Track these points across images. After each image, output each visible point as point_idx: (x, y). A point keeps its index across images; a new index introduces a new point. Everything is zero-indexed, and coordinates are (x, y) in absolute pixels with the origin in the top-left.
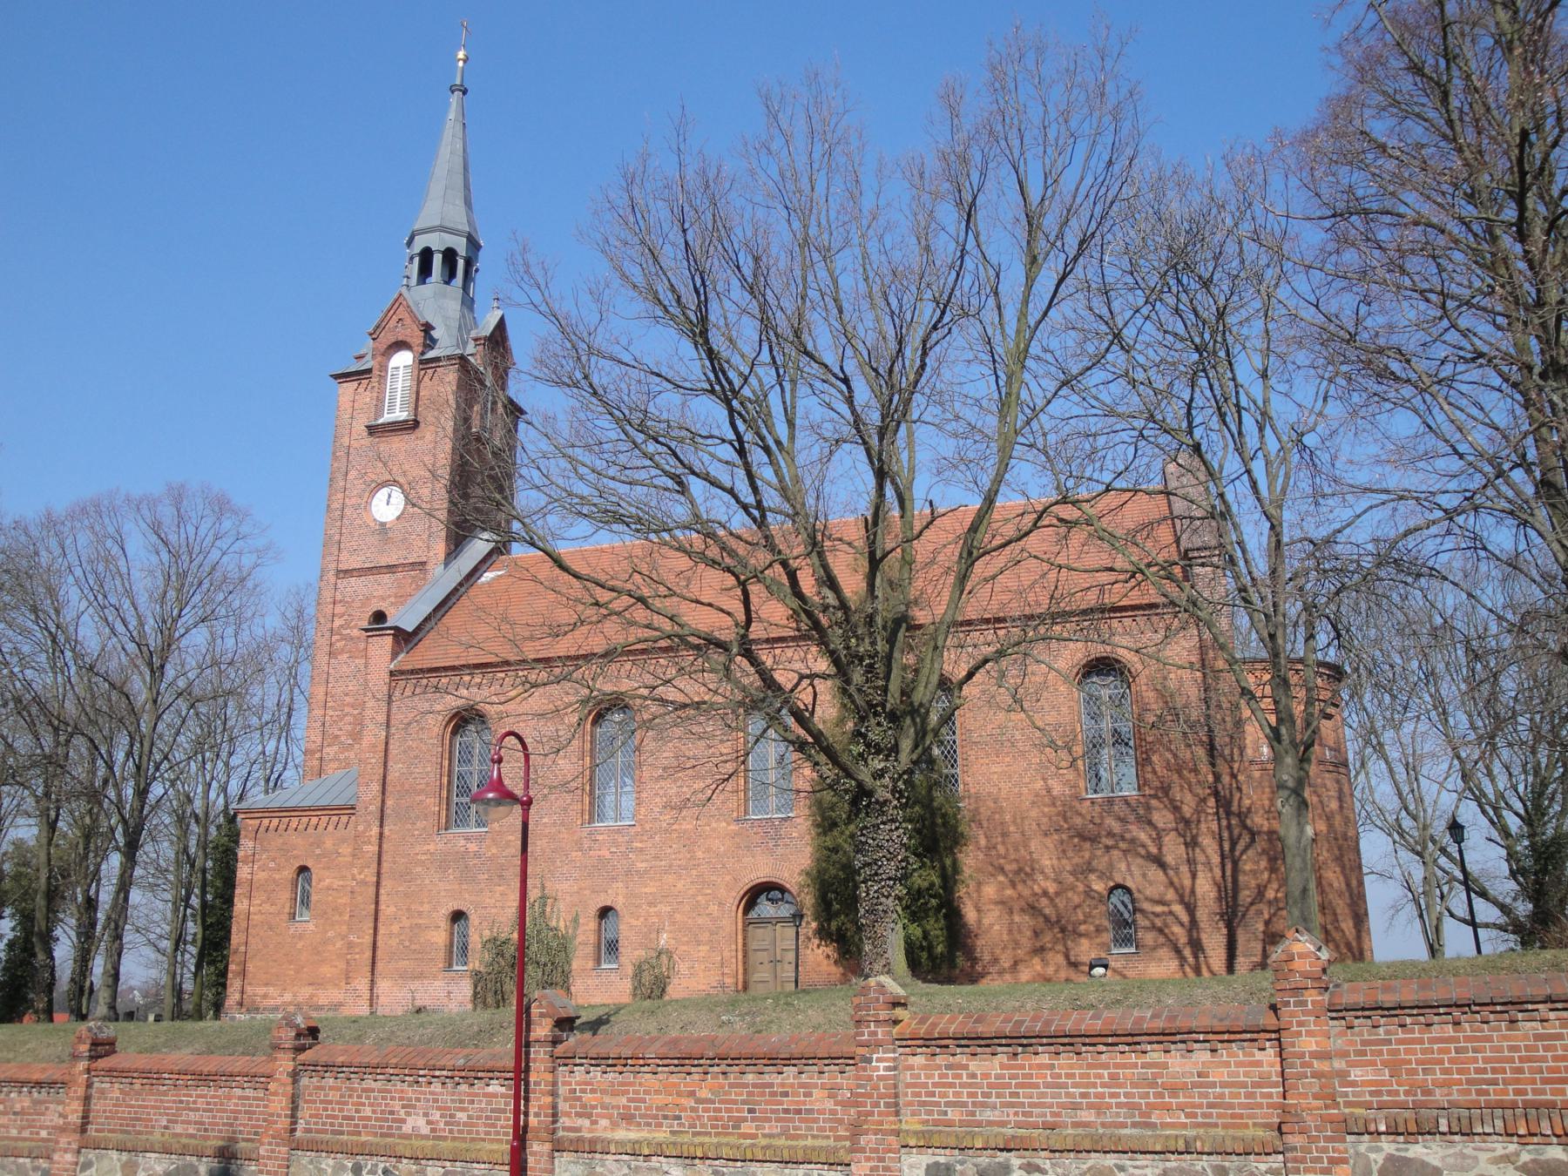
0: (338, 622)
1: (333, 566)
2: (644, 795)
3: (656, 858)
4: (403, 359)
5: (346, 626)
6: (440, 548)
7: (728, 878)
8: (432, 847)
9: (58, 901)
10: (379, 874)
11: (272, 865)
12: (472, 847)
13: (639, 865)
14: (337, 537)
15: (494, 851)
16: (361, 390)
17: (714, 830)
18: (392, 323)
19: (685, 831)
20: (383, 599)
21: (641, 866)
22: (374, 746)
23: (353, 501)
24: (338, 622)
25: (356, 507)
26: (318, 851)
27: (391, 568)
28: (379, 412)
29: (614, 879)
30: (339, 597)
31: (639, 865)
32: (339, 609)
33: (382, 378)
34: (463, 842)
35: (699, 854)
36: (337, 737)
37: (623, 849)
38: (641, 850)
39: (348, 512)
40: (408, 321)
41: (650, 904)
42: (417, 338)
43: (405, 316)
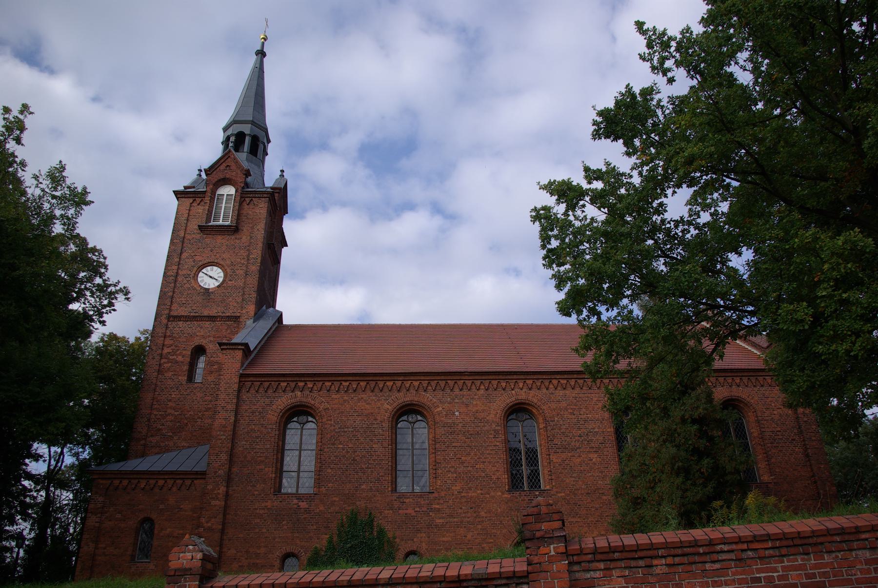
0: (166, 350)
1: (167, 312)
2: (440, 471)
3: (451, 516)
4: (228, 190)
5: (174, 353)
6: (251, 308)
7: (504, 531)
8: (269, 504)
9: (461, 578)
10: (224, 524)
11: (119, 516)
12: (303, 505)
13: (438, 521)
14: (170, 294)
15: (322, 508)
16: (195, 204)
17: (493, 497)
18: (222, 167)
19: (472, 497)
20: (203, 337)
21: (439, 521)
22: (224, 427)
23: (184, 272)
24: (166, 350)
25: (186, 276)
26: (161, 507)
27: (212, 318)
28: (208, 220)
29: (418, 531)
30: (168, 333)
31: (438, 521)
32: (168, 342)
33: (212, 199)
34: (295, 501)
35: (483, 514)
36: (160, 430)
37: (424, 509)
38: (439, 510)
39: (180, 279)
40: (234, 167)
41: (447, 549)
42: (240, 178)
43: (233, 164)
